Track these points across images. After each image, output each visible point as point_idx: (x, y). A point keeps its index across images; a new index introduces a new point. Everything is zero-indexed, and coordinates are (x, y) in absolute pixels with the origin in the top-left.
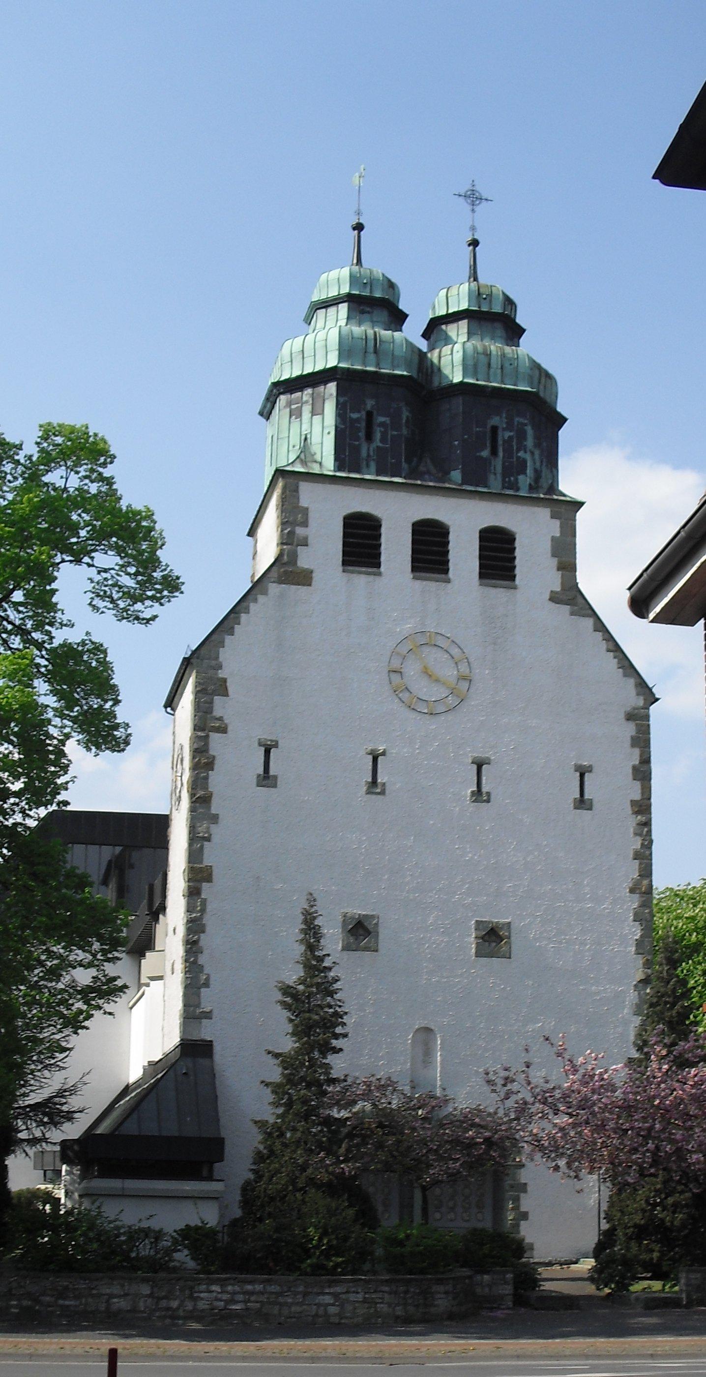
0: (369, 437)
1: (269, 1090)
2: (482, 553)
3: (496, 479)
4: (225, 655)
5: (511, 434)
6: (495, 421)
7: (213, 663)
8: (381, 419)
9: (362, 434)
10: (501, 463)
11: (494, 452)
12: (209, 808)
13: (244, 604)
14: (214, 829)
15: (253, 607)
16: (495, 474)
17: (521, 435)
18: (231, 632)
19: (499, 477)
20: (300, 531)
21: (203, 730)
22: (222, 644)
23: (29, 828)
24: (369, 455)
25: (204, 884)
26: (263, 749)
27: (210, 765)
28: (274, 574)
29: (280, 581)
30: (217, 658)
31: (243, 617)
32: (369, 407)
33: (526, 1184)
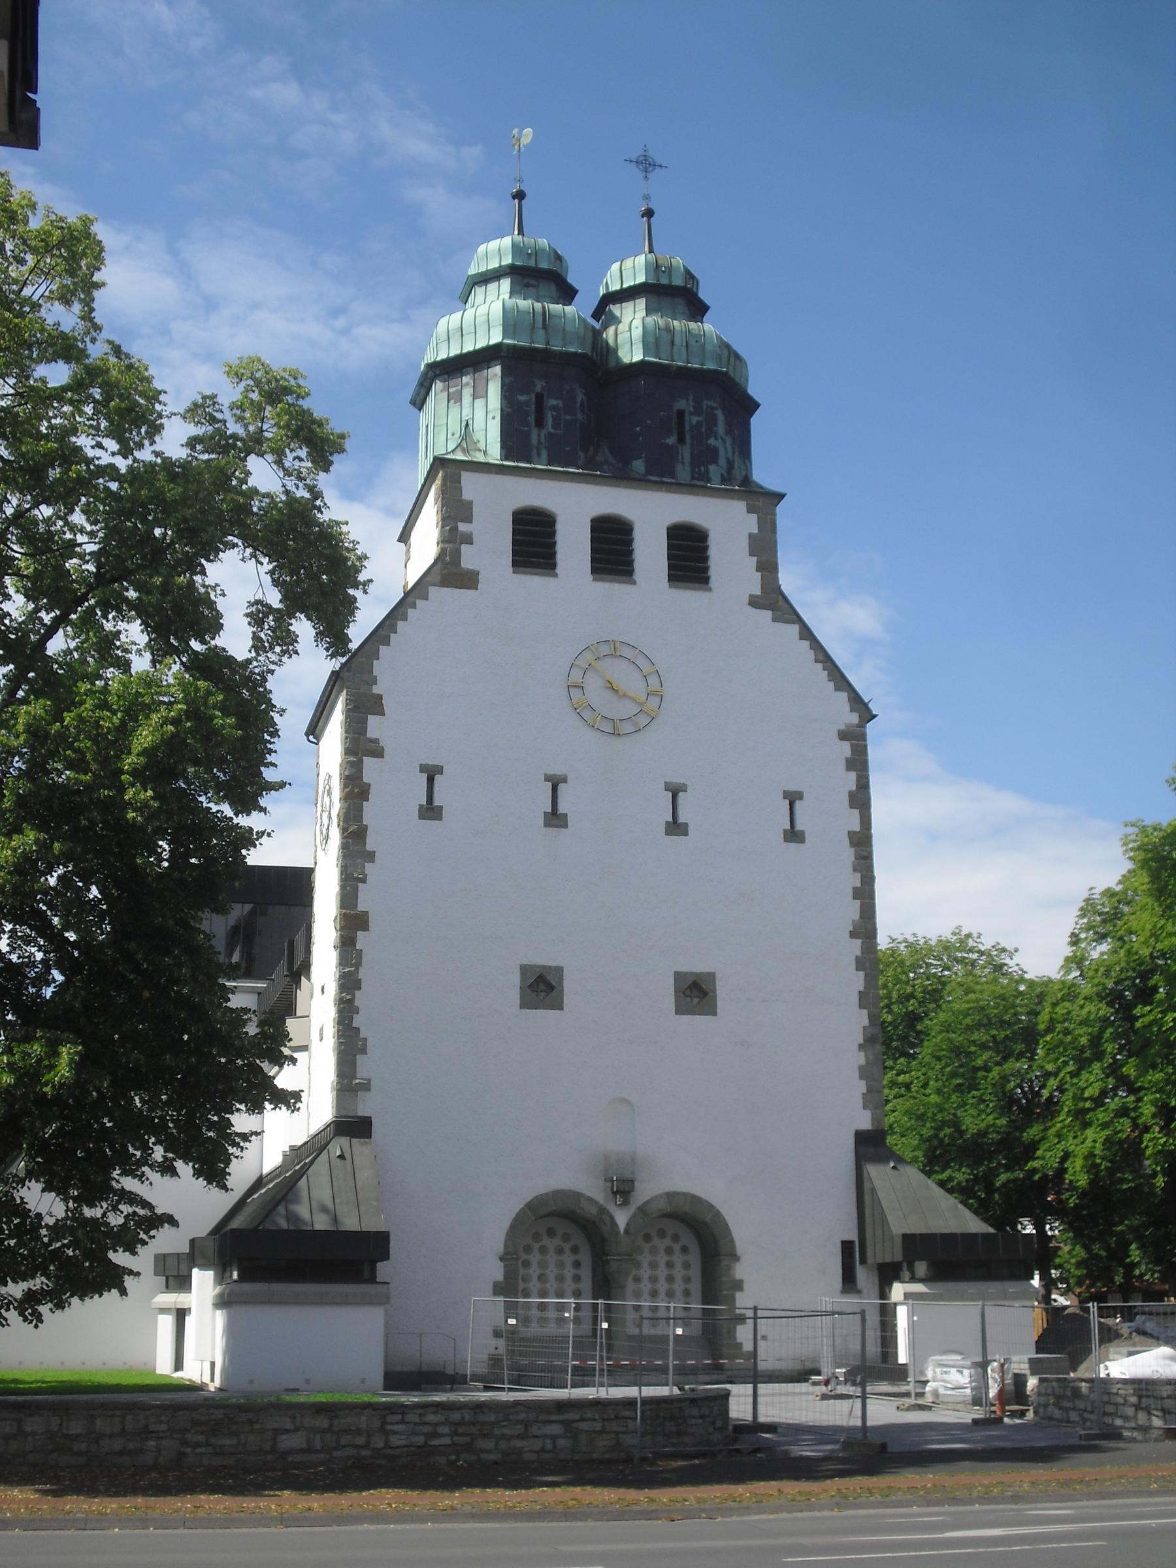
0: (540, 423)
6: (681, 404)
8: (553, 402)
9: (532, 419)
11: (681, 440)
14: (369, 868)
16: (683, 463)
18: (387, 642)
20: (463, 527)
24: (539, 443)
32: (538, 389)
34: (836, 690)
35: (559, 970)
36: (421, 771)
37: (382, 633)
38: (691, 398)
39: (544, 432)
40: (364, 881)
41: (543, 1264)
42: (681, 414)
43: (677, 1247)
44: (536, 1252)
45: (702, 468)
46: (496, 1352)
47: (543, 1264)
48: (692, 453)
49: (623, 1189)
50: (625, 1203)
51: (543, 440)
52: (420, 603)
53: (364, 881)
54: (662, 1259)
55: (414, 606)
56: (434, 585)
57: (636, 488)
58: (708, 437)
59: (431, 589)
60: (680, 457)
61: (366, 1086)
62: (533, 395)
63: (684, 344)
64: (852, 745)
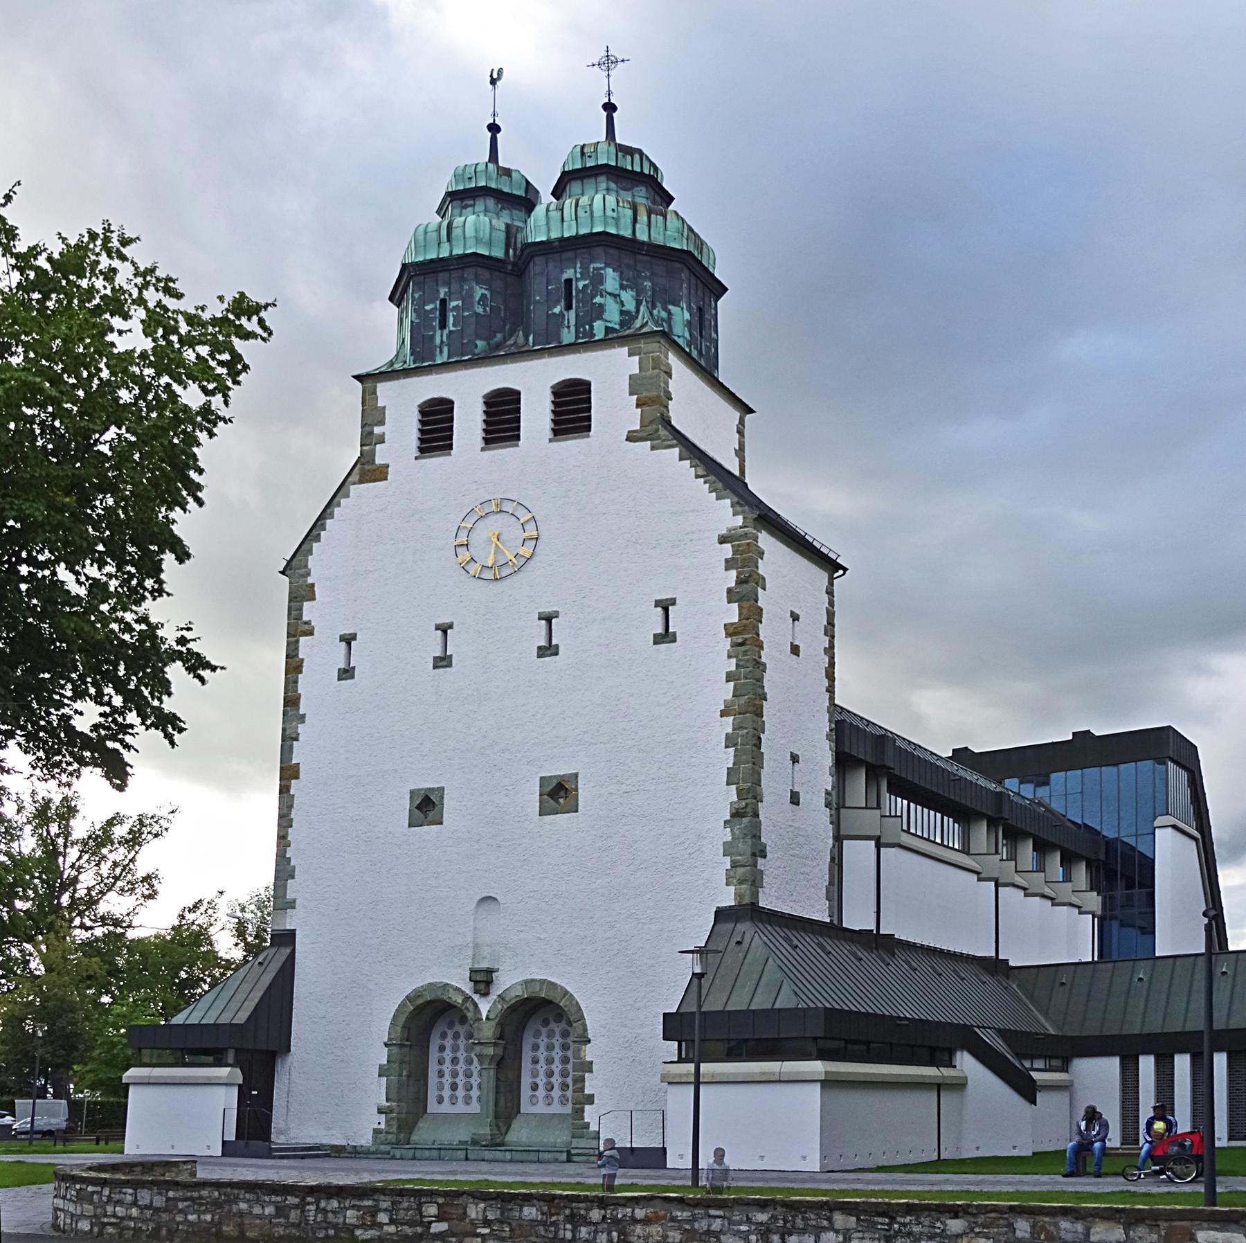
0: (443, 325)
1: (163, 576)
2: (123, 1100)
3: (569, 332)
4: (312, 561)
5: (587, 282)
6: (569, 274)
7: (302, 571)
8: (454, 304)
9: (436, 323)
10: (574, 315)
11: (569, 307)
12: (298, 709)
13: (329, 511)
14: (301, 729)
15: (337, 511)
16: (568, 327)
17: (598, 279)
18: (318, 539)
19: (573, 329)
20: (377, 430)
21: (294, 636)
22: (310, 552)
23: (761, 1224)
24: (442, 342)
25: (305, 603)
26: (464, 211)
27: (291, 807)
28: (354, 477)
29: (361, 481)
30: (306, 566)
31: (329, 522)
32: (442, 296)
33: (591, 1063)
34: (348, 496)
35: (413, 793)
36: (341, 641)
37: (315, 532)
38: (578, 265)
39: (446, 332)
40: (296, 739)
41: (455, 1049)
42: (569, 281)
43: (450, 1033)
44: (543, 1037)
45: (587, 327)
46: (380, 1127)
47: (455, 1049)
48: (577, 316)
49: (483, 980)
50: (485, 994)
51: (445, 339)
52: (343, 501)
53: (296, 739)
54: (448, 1043)
55: (339, 505)
56: (354, 484)
57: (521, 361)
58: (594, 297)
59: (352, 487)
60: (566, 322)
61: (292, 905)
62: (438, 302)
63: (574, 217)
64: (733, 546)
